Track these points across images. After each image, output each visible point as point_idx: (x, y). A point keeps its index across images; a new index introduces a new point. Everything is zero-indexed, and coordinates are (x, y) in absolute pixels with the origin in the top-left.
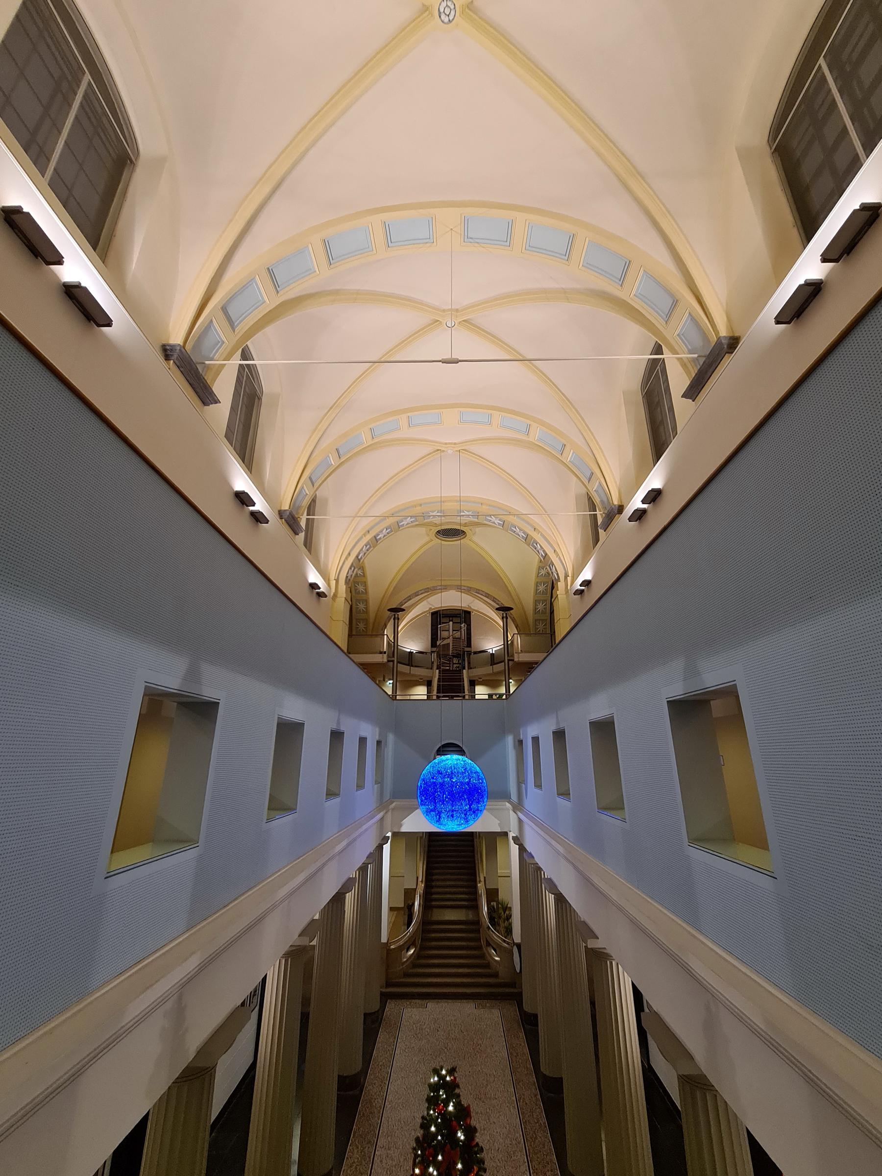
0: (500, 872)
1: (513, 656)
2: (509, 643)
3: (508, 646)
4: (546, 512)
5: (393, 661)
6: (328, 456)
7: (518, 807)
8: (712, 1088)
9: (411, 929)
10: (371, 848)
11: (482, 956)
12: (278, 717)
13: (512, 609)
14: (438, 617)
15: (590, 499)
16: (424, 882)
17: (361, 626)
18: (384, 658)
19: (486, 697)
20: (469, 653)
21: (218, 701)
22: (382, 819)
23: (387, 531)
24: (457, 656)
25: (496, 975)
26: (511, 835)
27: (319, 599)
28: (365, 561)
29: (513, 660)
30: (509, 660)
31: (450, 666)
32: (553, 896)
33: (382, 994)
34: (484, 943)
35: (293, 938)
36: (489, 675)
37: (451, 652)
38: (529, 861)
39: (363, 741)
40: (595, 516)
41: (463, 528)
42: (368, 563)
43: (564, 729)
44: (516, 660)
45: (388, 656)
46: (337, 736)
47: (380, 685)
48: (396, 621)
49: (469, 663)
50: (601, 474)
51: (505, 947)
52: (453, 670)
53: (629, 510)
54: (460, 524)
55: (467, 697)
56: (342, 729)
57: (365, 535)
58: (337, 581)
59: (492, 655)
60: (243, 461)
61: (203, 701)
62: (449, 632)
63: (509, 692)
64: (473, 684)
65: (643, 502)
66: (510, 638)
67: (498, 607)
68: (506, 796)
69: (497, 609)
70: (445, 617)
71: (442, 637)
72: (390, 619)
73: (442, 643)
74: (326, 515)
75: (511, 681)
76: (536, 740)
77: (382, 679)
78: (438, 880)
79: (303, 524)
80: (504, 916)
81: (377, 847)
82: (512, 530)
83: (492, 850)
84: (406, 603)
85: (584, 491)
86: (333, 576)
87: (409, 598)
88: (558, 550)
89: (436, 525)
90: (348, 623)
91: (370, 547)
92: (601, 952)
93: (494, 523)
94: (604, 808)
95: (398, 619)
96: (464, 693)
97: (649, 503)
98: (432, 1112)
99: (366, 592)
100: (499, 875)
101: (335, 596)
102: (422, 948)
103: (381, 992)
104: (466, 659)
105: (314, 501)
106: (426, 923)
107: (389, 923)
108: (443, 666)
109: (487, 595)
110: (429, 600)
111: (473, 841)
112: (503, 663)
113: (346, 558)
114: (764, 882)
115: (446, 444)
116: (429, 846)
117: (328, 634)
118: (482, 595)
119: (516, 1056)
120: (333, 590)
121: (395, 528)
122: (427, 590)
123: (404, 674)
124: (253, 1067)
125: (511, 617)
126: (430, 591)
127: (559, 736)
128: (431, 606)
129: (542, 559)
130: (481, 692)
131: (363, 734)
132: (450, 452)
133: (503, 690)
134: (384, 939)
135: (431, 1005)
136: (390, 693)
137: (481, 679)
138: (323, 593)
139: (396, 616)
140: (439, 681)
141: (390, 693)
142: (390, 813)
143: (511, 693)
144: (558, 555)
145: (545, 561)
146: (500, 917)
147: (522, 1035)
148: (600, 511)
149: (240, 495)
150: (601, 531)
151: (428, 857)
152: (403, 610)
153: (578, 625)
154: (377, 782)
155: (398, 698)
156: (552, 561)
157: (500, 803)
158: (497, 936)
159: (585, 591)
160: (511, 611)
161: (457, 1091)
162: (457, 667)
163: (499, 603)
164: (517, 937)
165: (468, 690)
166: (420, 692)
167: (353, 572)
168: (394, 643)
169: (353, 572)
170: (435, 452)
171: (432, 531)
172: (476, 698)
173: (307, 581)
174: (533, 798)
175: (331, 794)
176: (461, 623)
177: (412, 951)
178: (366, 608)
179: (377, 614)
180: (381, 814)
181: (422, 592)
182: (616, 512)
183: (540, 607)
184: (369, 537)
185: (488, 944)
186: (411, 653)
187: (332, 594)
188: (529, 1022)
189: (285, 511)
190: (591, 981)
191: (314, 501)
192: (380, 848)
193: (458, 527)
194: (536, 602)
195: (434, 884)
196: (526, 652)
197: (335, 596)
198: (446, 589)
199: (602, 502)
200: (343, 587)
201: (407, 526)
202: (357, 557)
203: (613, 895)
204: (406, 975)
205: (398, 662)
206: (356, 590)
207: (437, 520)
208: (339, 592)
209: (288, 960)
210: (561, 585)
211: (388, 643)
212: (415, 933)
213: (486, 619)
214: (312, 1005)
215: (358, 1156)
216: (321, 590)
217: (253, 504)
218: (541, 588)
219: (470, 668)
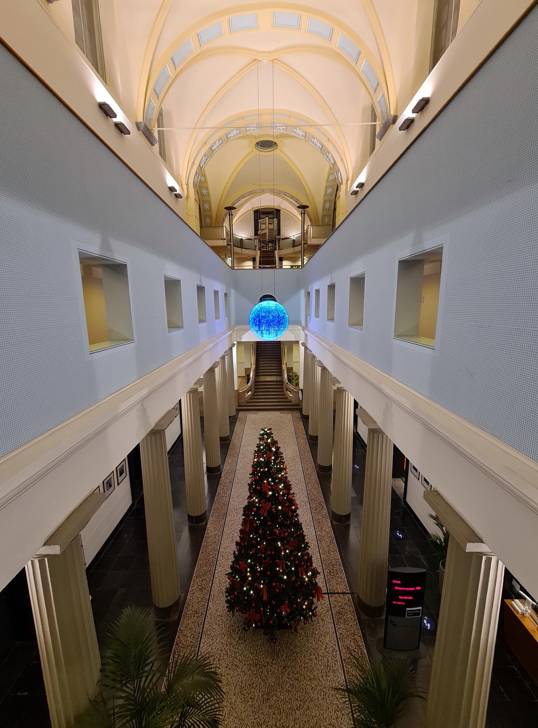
0: (294, 360)
1: (307, 240)
3: (304, 234)
4: (338, 123)
5: (230, 245)
6: (166, 66)
7: (305, 328)
9: (249, 384)
10: (227, 348)
11: (284, 395)
13: (307, 207)
14: (259, 214)
15: (373, 110)
17: (208, 220)
18: (225, 243)
19: (289, 267)
20: (279, 240)
23: (219, 143)
24: (271, 241)
25: (291, 402)
26: (300, 342)
28: (206, 169)
29: (307, 244)
30: (304, 244)
31: (266, 249)
33: (237, 410)
34: (285, 389)
35: (191, 385)
36: (292, 253)
37: (267, 239)
38: (309, 353)
39: (216, 293)
40: (375, 125)
41: (275, 140)
42: (207, 170)
45: (227, 242)
46: (201, 289)
47: (224, 260)
48: (231, 216)
49: (279, 246)
50: (386, 86)
51: (295, 391)
52: (269, 251)
53: (400, 121)
54: (273, 136)
55: (277, 267)
56: (204, 285)
57: (203, 146)
59: (294, 240)
60: (97, 70)
61: (117, 263)
62: (266, 225)
63: (304, 264)
64: (281, 259)
65: (414, 111)
67: (298, 205)
68: (298, 323)
69: (298, 207)
70: (263, 214)
72: (227, 215)
73: (262, 233)
74: (172, 127)
75: (305, 257)
76: (318, 291)
77: (225, 257)
79: (156, 135)
80: (295, 378)
82: (312, 141)
83: (290, 350)
84: (236, 203)
85: (369, 103)
86: (184, 182)
87: (238, 200)
88: (344, 159)
89: (255, 137)
90: (199, 218)
91: (208, 157)
93: (299, 134)
95: (232, 215)
97: (418, 113)
98: (261, 442)
101: (188, 197)
102: (255, 392)
104: (277, 243)
105: (161, 114)
106: (256, 382)
107: (238, 383)
108: (262, 248)
109: (292, 197)
110: (252, 200)
113: (192, 167)
114: (429, 351)
115: (262, 52)
116: (257, 348)
117: (186, 222)
118: (288, 197)
120: (186, 193)
121: (225, 140)
122: (251, 193)
123: (237, 253)
124: (181, 434)
125: (307, 214)
126: (253, 193)
127: (332, 287)
128: (253, 206)
130: (286, 264)
131: (217, 289)
132: (265, 62)
133: (299, 263)
134: (236, 388)
135: (260, 413)
136: (230, 265)
137: (286, 256)
139: (231, 213)
140: (260, 258)
141: (230, 265)
142: (235, 332)
144: (343, 163)
145: (334, 169)
146: (293, 379)
147: (301, 422)
148: (379, 121)
149: (103, 106)
150: (377, 140)
151: (257, 353)
152: (235, 208)
154: (226, 316)
155: (235, 268)
157: (296, 327)
158: (291, 387)
159: (359, 192)
160: (307, 209)
161: (272, 436)
162: (271, 249)
163: (300, 202)
164: (301, 386)
166: (249, 265)
167: (198, 178)
168: (230, 232)
169: (198, 178)
170: (252, 62)
171: (252, 143)
173: (93, 99)
174: (314, 322)
175: (173, 326)
176: (273, 218)
177: (250, 393)
178: (210, 207)
179: (218, 210)
180: (230, 332)
181: (247, 194)
182: (391, 122)
184: (207, 147)
185: (287, 390)
186: (241, 240)
188: (305, 419)
189: (140, 123)
190: (335, 403)
191: (161, 114)
192: (231, 349)
193: (271, 139)
194: (325, 202)
196: (317, 238)
197: (188, 197)
199: (382, 112)
200: (192, 191)
201: (234, 138)
202: (199, 165)
203: (351, 364)
204: (247, 402)
205: (234, 246)
207: (256, 132)
210: (343, 188)
211: (227, 233)
213: (291, 215)
214: (204, 413)
216: (178, 192)
217: (115, 116)
218: (329, 191)
219: (279, 249)
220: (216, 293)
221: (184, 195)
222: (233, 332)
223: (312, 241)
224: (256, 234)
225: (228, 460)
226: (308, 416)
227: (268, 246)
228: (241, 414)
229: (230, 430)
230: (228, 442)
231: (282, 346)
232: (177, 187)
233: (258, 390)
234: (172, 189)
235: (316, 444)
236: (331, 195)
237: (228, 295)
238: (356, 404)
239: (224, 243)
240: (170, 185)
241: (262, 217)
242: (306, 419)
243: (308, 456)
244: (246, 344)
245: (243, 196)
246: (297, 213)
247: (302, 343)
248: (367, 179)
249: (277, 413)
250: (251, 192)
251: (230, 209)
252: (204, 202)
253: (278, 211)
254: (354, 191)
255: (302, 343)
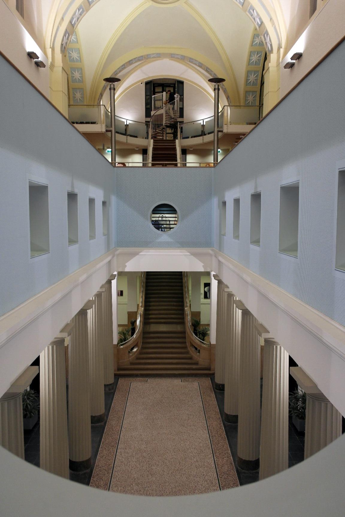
1: (222, 127)
2: (220, 114)
3: (218, 117)
8: (327, 400)
9: (135, 336)
11: (188, 353)
12: (29, 182)
13: (222, 80)
16: (143, 307)
17: (78, 95)
21: (47, 185)
22: (110, 262)
25: (197, 364)
26: (213, 273)
27: (38, 69)
32: (241, 311)
34: (188, 344)
37: (164, 122)
39: (92, 201)
43: (260, 193)
44: (225, 131)
45: (107, 126)
46: (72, 197)
47: (101, 151)
52: (166, 140)
55: (179, 165)
56: (76, 191)
58: (53, 49)
63: (217, 161)
64: (185, 152)
66: (220, 109)
67: (211, 78)
69: (211, 80)
71: (157, 106)
72: (106, 88)
75: (219, 150)
76: (237, 201)
78: (154, 306)
81: (106, 282)
86: (48, 44)
90: (67, 95)
92: (269, 340)
94: (283, 250)
95: (114, 89)
96: (176, 161)
99: (80, 60)
100: (201, 303)
101: (52, 65)
102: (143, 348)
103: (114, 373)
106: (145, 333)
109: (201, 65)
111: (182, 279)
112: (213, 134)
113: (60, 24)
119: (208, 406)
120: (50, 60)
125: (222, 88)
127: (256, 197)
129: (258, 27)
131: (92, 196)
137: (191, 148)
138: (41, 62)
141: (110, 161)
142: (115, 257)
143: (219, 161)
144: (273, 24)
147: (213, 395)
151: (146, 290)
152: (118, 80)
153: (268, 117)
156: (267, 31)
165: (180, 158)
172: (187, 166)
175: (72, 241)
183: (252, 78)
187: (49, 63)
188: (219, 389)
192: (109, 282)
194: (248, 73)
195: (151, 308)
198: (160, 57)
200: (59, 56)
202: (71, 22)
204: (132, 364)
206: (70, 57)
208: (56, 62)
209: (54, 346)
210: (273, 57)
212: (137, 339)
213: (199, 91)
215: (106, 453)
216: (40, 59)
218: (254, 58)
220: (92, 201)
221: (48, 63)
222: (113, 257)
223: (230, 129)
224: (148, 113)
225: (103, 452)
226: (223, 386)
227: (165, 133)
228: (121, 381)
229: (106, 405)
230: (102, 424)
231: (184, 280)
232: (38, 52)
233: (148, 345)
234: (31, 55)
235: (236, 429)
236: (257, 63)
237: (107, 203)
238: (292, 363)
239: (99, 128)
240: (29, 49)
241: (157, 90)
242: (220, 390)
243: (223, 446)
244: (131, 276)
245: (130, 63)
246: (209, 89)
247: (214, 275)
248: (307, 48)
249: (177, 382)
250: (142, 56)
251: (112, 80)
252: (73, 69)
253: (181, 83)
254: (288, 64)
255: (214, 275)
